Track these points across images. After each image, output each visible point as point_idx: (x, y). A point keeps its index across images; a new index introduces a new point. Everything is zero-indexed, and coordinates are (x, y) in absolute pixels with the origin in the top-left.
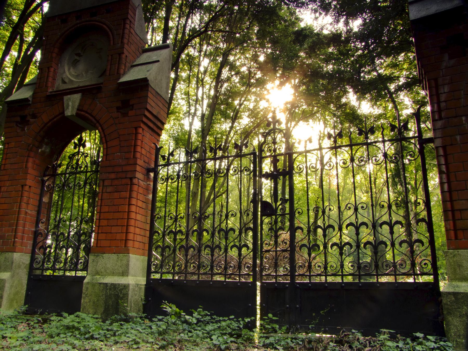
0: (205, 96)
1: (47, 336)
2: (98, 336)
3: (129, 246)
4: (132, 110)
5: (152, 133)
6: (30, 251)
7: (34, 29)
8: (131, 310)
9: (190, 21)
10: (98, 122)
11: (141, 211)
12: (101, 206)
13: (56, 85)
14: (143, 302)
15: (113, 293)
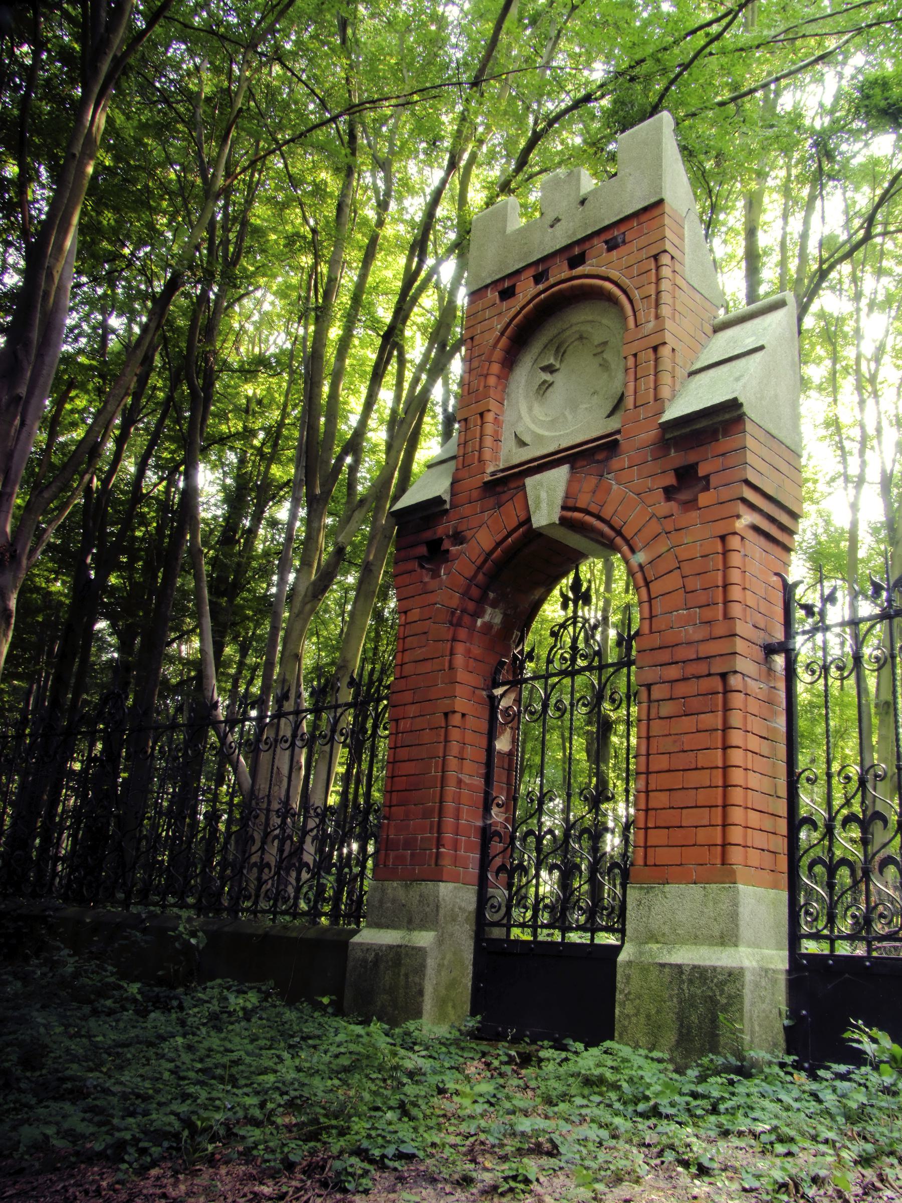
0: (885, 424)
1: (539, 1100)
2: (671, 1111)
3: (733, 861)
4: (707, 488)
5: (770, 546)
6: (475, 880)
7: (423, 328)
8: (752, 1042)
9: (815, 217)
10: (619, 533)
11: (759, 764)
12: (648, 755)
13: (503, 454)
14: (786, 1022)
15: (699, 992)
